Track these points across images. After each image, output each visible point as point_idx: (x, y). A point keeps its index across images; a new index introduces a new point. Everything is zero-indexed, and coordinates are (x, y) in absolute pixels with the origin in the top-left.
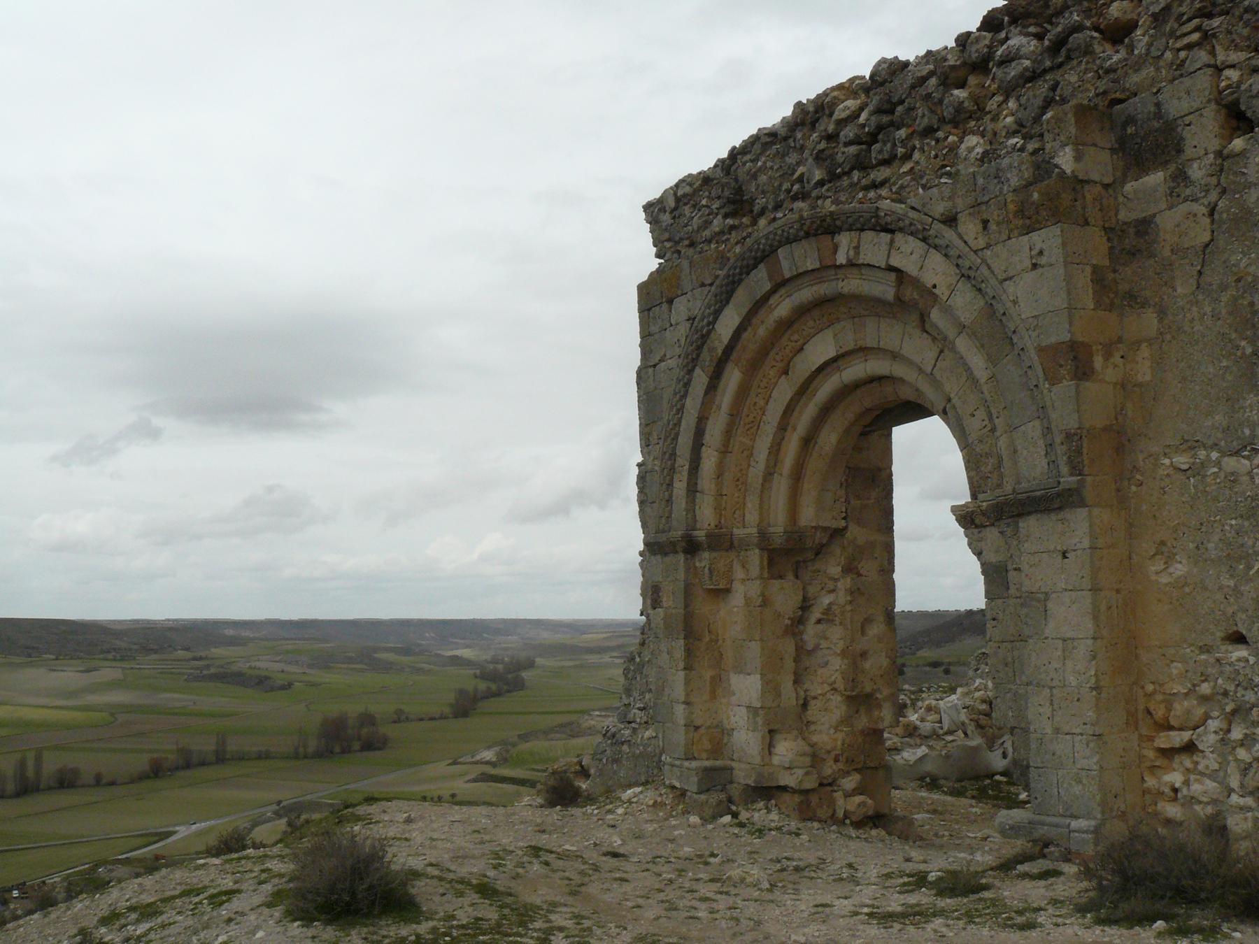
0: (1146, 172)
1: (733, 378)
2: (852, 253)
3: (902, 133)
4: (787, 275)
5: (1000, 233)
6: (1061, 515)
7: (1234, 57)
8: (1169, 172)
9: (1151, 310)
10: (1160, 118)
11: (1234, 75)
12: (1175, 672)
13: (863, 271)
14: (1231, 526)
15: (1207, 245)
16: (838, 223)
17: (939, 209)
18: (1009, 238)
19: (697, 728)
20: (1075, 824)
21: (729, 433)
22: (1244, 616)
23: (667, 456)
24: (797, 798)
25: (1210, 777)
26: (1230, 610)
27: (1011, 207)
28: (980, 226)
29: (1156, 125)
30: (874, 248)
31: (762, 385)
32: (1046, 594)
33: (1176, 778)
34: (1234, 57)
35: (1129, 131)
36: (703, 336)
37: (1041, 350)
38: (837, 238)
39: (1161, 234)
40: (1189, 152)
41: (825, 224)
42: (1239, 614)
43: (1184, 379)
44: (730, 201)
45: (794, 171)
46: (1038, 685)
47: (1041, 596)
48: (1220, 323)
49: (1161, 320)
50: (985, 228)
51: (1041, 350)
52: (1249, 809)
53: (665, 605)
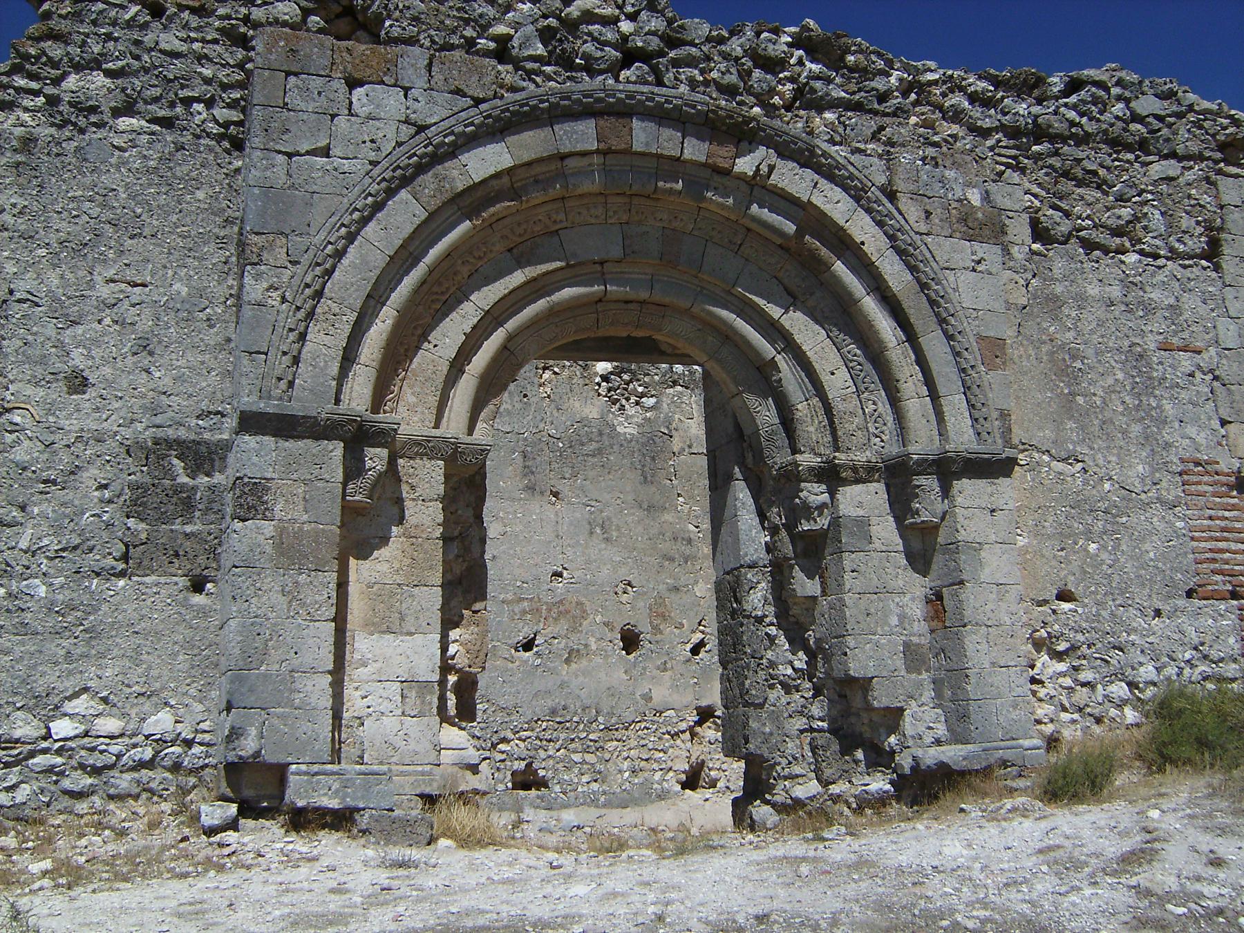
26: (1063, 574)
28: (923, 216)
30: (792, 179)
50: (927, 218)
51: (980, 338)
53: (278, 514)
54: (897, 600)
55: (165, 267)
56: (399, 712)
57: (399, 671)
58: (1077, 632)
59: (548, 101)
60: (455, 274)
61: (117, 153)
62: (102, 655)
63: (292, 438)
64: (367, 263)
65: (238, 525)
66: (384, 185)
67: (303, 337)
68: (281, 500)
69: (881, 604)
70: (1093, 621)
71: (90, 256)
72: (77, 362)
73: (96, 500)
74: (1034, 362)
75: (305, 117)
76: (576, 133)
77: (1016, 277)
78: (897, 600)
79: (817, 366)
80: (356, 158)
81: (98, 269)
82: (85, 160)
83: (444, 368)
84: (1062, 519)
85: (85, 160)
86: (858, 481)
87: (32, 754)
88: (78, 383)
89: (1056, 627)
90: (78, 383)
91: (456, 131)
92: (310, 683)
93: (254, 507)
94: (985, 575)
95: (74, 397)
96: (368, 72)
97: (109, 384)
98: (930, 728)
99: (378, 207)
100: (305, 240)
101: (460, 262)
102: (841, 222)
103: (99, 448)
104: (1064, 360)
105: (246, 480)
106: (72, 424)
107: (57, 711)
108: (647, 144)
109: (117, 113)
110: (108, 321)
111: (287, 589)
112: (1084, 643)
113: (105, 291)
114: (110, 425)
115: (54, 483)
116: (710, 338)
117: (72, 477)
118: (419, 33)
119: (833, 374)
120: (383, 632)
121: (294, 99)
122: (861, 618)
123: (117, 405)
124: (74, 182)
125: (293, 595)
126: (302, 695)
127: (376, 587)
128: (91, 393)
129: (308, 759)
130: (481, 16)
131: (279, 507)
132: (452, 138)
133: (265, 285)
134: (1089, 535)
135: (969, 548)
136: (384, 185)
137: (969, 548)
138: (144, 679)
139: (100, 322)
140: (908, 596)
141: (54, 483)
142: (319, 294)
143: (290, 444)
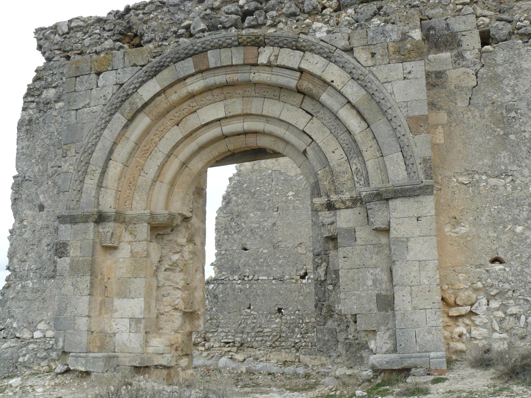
0: (441, 51)
1: (143, 121)
2: (272, 58)
3: (274, 13)
4: (212, 65)
5: (383, 60)
6: (417, 199)
7: (486, 12)
8: (454, 54)
9: (443, 112)
10: (449, 30)
11: (487, 20)
12: (461, 278)
13: (273, 70)
14: (495, 209)
15: (475, 87)
16: (266, 41)
17: (343, 44)
18: (389, 63)
19: (92, 332)
20: (432, 355)
21: (131, 154)
22: (502, 250)
23: (83, 164)
24: (165, 372)
25: (481, 327)
26: (494, 247)
27: (391, 49)
28: (370, 56)
29: (446, 32)
30: (289, 58)
31: (160, 129)
32: (407, 238)
33: (462, 329)
34: (486, 12)
35: (431, 32)
36: (128, 95)
37: (408, 118)
38: (261, 49)
39: (449, 79)
40: (465, 46)
41: (258, 40)
42: (500, 249)
43: (465, 143)
44: (120, 33)
45: (182, 22)
46: (402, 285)
47: (405, 240)
48: (484, 120)
49: (449, 116)
50: (372, 57)
51: (408, 118)
52: (505, 339)
53: (71, 254)
54: (372, 271)
56: (128, 331)
67: (82, 181)
68: (72, 249)
69: (361, 274)
70: (518, 276)
74: (479, 119)
76: (185, 67)
77: (468, 70)
78: (372, 271)
80: (98, 105)
82: (45, 123)
87: (29, 343)
89: (489, 280)
94: (410, 256)
96: (103, 67)
100: (81, 143)
104: (502, 114)
107: (35, 329)
108: (216, 63)
109: (56, 102)
112: (509, 290)
118: (155, 36)
119: (334, 152)
120: (123, 298)
121: (78, 88)
128: (46, 210)
129: (78, 351)
130: (178, 20)
131: (72, 251)
133: (68, 164)
134: (516, 222)
136: (108, 113)
142: (88, 163)
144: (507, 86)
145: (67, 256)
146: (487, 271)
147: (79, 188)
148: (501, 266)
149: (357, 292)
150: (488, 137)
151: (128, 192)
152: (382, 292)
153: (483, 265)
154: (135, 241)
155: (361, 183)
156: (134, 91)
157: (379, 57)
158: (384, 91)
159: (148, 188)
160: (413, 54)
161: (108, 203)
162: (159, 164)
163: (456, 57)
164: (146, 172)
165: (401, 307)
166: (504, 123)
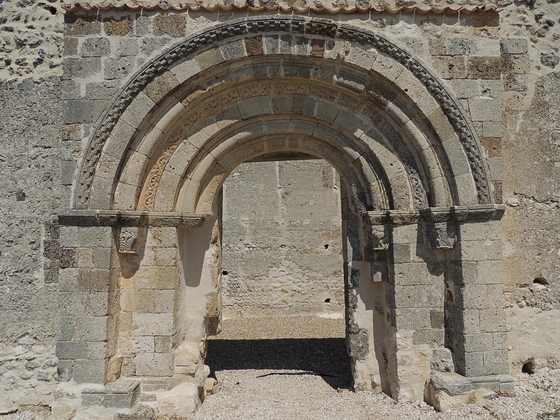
22: (545, 271)
28: (447, 68)
32: (477, 261)
40: (516, 70)
50: (450, 69)
53: (79, 264)
54: (427, 288)
55: (58, 138)
57: (154, 331)
58: (546, 302)
59: (215, 33)
60: (181, 131)
61: (36, 85)
62: (33, 318)
63: (86, 226)
64: (124, 133)
65: (61, 271)
66: (129, 91)
71: (26, 136)
72: (20, 186)
73: (30, 249)
75: (89, 60)
78: (427, 288)
79: (382, 161)
81: (30, 141)
83: (178, 180)
84: (541, 237)
85: (22, 90)
86: (404, 224)
88: (21, 196)
90: (21, 196)
91: (166, 57)
92: (94, 347)
93: (68, 262)
94: (480, 279)
95: (20, 202)
97: (34, 196)
98: (442, 361)
99: (128, 103)
101: (183, 125)
102: (392, 79)
103: (30, 225)
104: (548, 141)
105: (64, 248)
106: (19, 215)
110: (33, 166)
111: (84, 301)
113: (33, 152)
114: (35, 215)
115: (12, 242)
116: (326, 149)
117: (20, 239)
119: (392, 165)
122: (404, 299)
123: (38, 205)
124: (18, 101)
125: (87, 304)
126: (91, 352)
127: (143, 290)
128: (27, 200)
131: (80, 261)
132: (164, 61)
135: (469, 264)
136: (129, 91)
137: (469, 264)
138: (51, 329)
139: (29, 166)
140: (434, 286)
141: (12, 242)
143: (85, 229)
144: (552, 114)
145: (73, 267)
146: (532, 291)
147: (88, 181)
148: (543, 287)
149: (411, 309)
150: (536, 163)
151: (150, 188)
152: (436, 309)
153: (528, 285)
154: (161, 247)
155: (421, 199)
156: (165, 67)
157: (457, 70)
158: (460, 107)
159: (175, 186)
160: (491, 72)
161: (125, 202)
162: (190, 159)
163: (508, 79)
164: (173, 167)
165: (471, 330)
166: (550, 150)
